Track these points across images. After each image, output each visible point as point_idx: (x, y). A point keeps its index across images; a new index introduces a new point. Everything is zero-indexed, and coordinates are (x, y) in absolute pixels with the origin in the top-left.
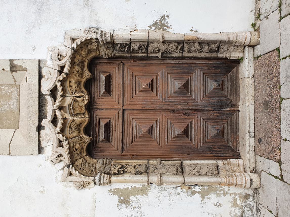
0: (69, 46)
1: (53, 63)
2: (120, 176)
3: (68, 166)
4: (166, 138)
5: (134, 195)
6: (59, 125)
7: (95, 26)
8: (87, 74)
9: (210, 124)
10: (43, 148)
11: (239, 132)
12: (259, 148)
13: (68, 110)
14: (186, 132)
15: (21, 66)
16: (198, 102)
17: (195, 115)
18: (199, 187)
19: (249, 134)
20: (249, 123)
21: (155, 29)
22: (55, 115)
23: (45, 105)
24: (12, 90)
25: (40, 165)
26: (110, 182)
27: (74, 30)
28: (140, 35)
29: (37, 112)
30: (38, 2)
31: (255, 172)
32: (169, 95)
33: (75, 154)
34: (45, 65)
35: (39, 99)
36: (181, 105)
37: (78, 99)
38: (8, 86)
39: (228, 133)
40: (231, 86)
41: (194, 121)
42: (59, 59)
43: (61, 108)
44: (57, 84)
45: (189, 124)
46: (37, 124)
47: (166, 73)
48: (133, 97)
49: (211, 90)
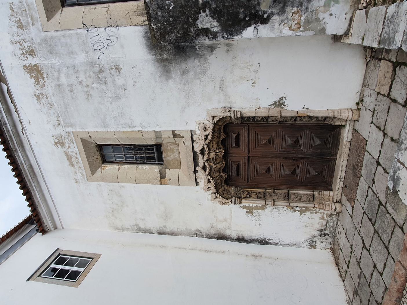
0: (211, 122)
1: (201, 132)
2: (247, 199)
3: (215, 194)
4: (279, 175)
5: (256, 210)
6: (208, 171)
7: (229, 106)
8: (223, 136)
9: (312, 167)
10: (198, 182)
11: (334, 173)
12: (345, 190)
13: (212, 161)
14: (294, 172)
15: (180, 135)
16: (305, 152)
17: (302, 161)
18: (299, 208)
19: (340, 180)
20: (341, 173)
21: (274, 107)
22: (204, 164)
23: (198, 159)
24: (174, 146)
25: (197, 191)
26: (241, 202)
27: (213, 109)
28: (262, 113)
29: (193, 163)
30: (186, 90)
31: (340, 202)
32: (283, 147)
33: (218, 186)
34: (195, 134)
35: (194, 159)
36: (292, 154)
37: (218, 153)
38: (171, 144)
39: (325, 173)
40: (332, 141)
41: (300, 164)
42: (204, 130)
43: (207, 160)
44: (205, 147)
45: (297, 166)
46: (193, 170)
47: (282, 132)
48: (255, 148)
49: (316, 144)
